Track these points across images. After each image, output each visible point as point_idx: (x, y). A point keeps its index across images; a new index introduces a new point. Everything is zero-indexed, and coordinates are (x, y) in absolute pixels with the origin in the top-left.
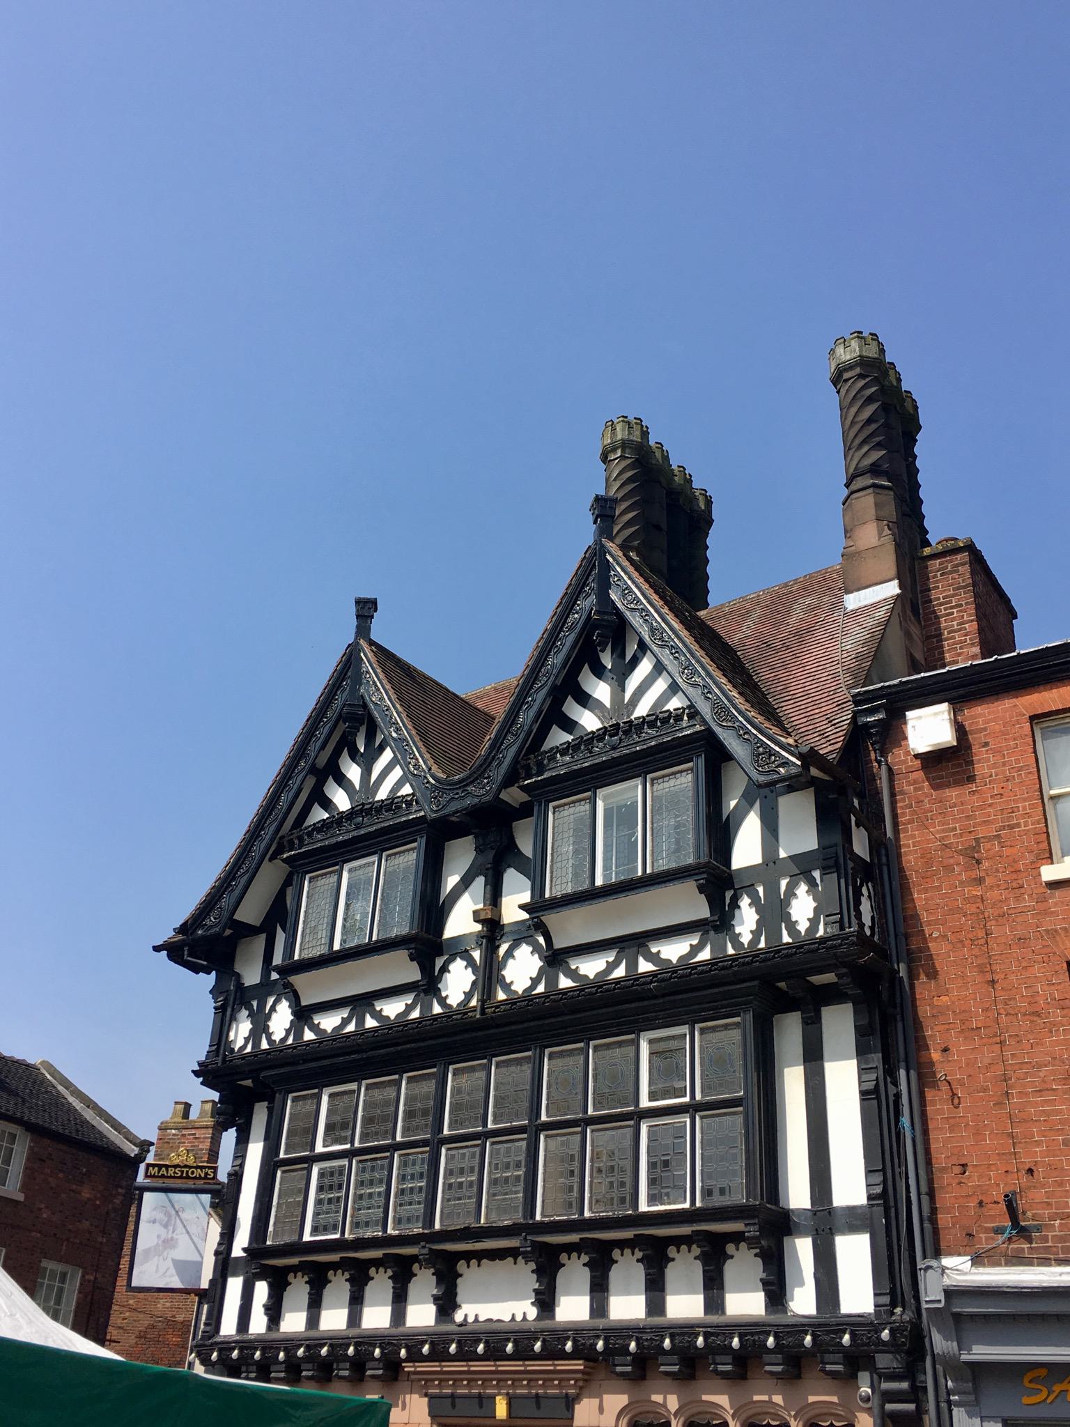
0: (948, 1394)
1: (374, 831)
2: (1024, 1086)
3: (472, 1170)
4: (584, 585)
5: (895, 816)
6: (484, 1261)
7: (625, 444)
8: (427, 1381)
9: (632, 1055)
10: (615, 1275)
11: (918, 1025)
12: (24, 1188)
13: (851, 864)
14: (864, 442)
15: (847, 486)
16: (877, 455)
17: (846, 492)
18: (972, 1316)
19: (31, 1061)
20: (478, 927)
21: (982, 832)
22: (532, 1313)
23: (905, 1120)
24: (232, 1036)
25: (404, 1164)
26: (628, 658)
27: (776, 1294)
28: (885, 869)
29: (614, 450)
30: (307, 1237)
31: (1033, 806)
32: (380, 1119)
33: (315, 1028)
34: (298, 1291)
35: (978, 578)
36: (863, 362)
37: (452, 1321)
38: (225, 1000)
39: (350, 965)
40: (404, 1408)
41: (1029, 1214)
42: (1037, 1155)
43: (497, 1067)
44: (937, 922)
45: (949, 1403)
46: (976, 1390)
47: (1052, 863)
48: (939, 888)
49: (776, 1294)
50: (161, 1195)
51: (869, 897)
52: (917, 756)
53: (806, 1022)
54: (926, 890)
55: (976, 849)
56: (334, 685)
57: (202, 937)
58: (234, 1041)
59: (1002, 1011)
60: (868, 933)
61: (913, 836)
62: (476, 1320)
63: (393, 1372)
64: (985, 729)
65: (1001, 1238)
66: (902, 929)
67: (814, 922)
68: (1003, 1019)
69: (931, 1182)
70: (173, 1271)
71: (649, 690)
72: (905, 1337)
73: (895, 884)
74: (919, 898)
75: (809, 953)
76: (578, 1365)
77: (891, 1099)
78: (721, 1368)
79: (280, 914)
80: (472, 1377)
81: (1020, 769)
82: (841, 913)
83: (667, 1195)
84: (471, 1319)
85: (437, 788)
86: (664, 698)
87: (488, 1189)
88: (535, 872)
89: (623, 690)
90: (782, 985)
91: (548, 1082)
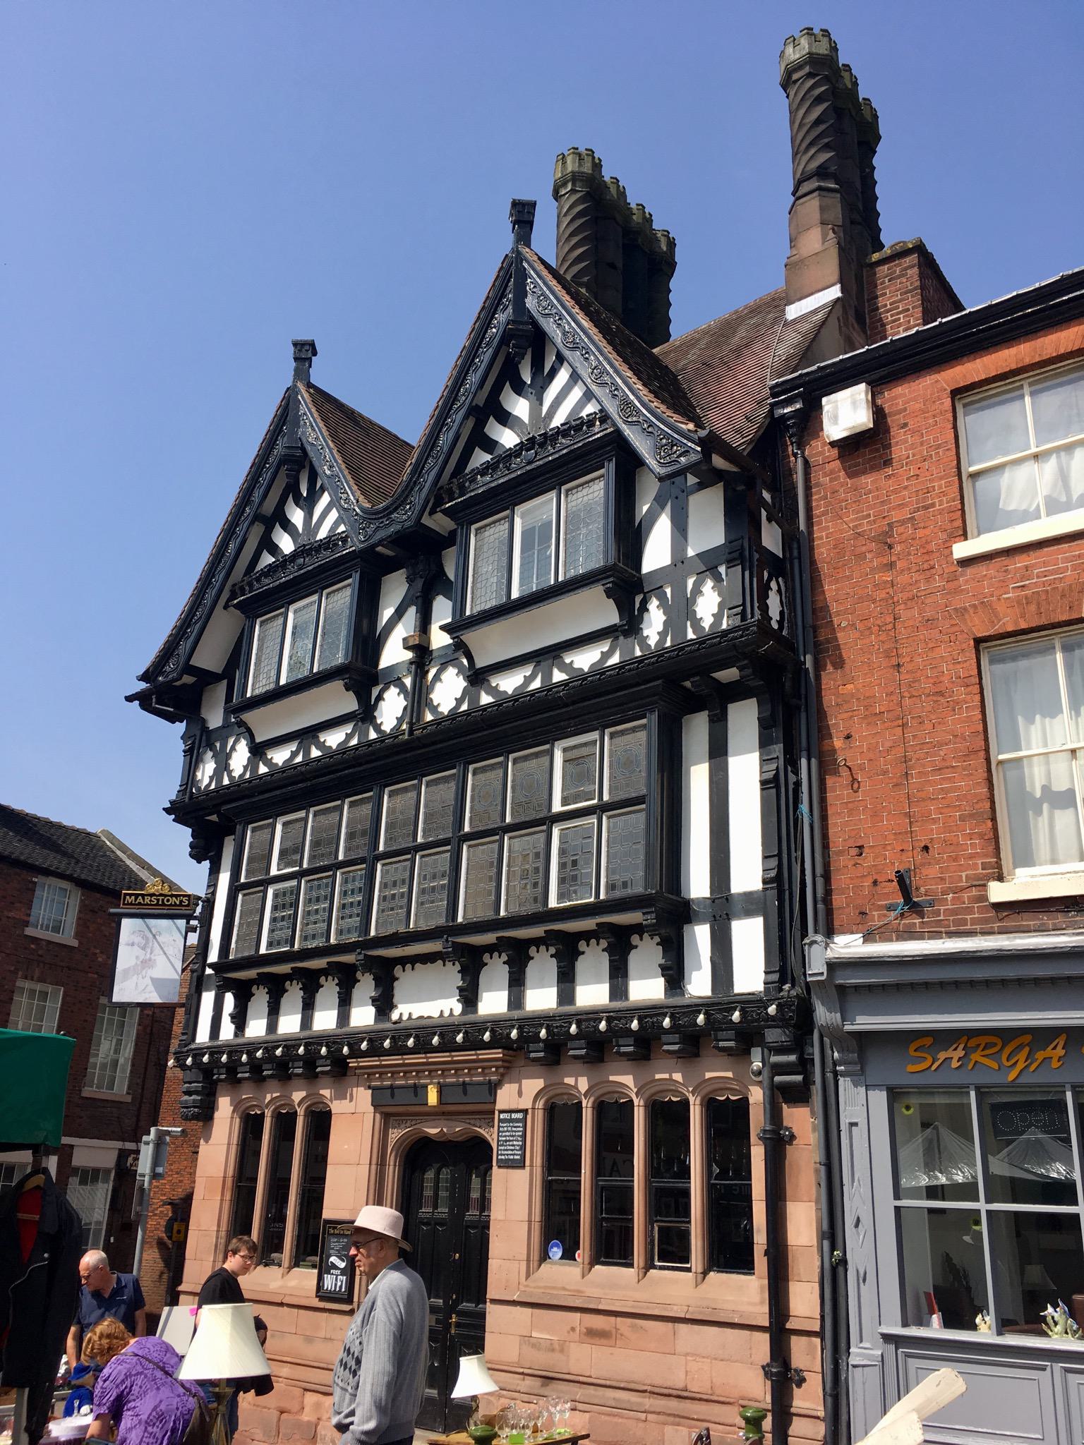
0: (835, 1064)
1: (315, 571)
2: (924, 766)
3: (403, 882)
4: (503, 296)
5: (809, 510)
6: (418, 965)
7: (575, 177)
8: (369, 1074)
9: (547, 764)
10: (532, 970)
11: (822, 714)
12: (78, 935)
13: (756, 556)
14: (811, 144)
15: (793, 194)
16: (824, 157)
17: (793, 199)
18: (857, 988)
19: (91, 829)
20: (409, 655)
21: (896, 516)
22: (458, 1008)
23: (804, 807)
24: (199, 775)
25: (345, 881)
26: (547, 370)
27: (675, 976)
28: (796, 562)
29: (564, 184)
30: (263, 951)
31: (949, 484)
32: (325, 842)
33: (268, 763)
34: (260, 1000)
35: (928, 282)
36: (813, 60)
37: (389, 1019)
38: (193, 743)
39: (293, 699)
40: (351, 1100)
41: (922, 890)
42: (932, 832)
43: (427, 786)
44: (846, 612)
45: (836, 1074)
46: (862, 1061)
47: (966, 539)
48: (850, 578)
49: (675, 976)
50: (139, 921)
51: (779, 591)
52: (833, 444)
53: (712, 720)
54: (837, 581)
55: (889, 534)
56: (275, 431)
57: (163, 683)
58: (201, 781)
59: (906, 694)
60: (775, 626)
61: (827, 528)
62: (410, 1017)
63: (340, 1071)
64: (905, 409)
65: (893, 914)
66: (810, 621)
67: (718, 617)
68: (907, 701)
69: (827, 866)
70: (151, 988)
71: (564, 400)
72: (793, 1011)
73: (806, 577)
74: (829, 589)
75: (713, 650)
76: (497, 1054)
77: (791, 787)
78: (623, 1049)
79: (238, 657)
80: (407, 1070)
81: (939, 447)
82: (744, 604)
83: (575, 892)
84: (405, 1017)
85: (364, 519)
86: (580, 405)
87: (418, 898)
88: (457, 593)
89: (541, 404)
90: (688, 684)
91: (472, 797)
